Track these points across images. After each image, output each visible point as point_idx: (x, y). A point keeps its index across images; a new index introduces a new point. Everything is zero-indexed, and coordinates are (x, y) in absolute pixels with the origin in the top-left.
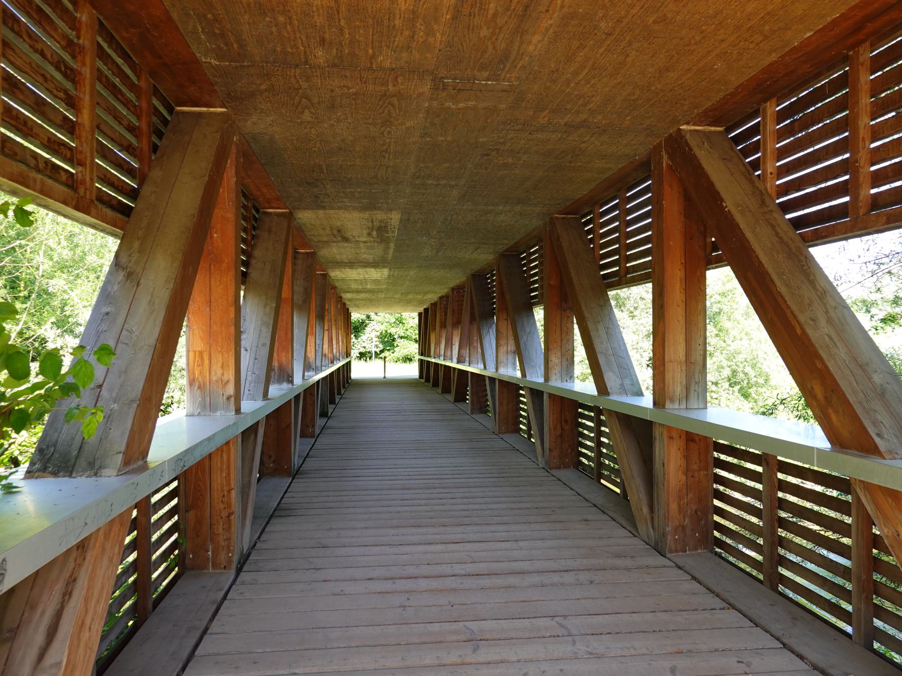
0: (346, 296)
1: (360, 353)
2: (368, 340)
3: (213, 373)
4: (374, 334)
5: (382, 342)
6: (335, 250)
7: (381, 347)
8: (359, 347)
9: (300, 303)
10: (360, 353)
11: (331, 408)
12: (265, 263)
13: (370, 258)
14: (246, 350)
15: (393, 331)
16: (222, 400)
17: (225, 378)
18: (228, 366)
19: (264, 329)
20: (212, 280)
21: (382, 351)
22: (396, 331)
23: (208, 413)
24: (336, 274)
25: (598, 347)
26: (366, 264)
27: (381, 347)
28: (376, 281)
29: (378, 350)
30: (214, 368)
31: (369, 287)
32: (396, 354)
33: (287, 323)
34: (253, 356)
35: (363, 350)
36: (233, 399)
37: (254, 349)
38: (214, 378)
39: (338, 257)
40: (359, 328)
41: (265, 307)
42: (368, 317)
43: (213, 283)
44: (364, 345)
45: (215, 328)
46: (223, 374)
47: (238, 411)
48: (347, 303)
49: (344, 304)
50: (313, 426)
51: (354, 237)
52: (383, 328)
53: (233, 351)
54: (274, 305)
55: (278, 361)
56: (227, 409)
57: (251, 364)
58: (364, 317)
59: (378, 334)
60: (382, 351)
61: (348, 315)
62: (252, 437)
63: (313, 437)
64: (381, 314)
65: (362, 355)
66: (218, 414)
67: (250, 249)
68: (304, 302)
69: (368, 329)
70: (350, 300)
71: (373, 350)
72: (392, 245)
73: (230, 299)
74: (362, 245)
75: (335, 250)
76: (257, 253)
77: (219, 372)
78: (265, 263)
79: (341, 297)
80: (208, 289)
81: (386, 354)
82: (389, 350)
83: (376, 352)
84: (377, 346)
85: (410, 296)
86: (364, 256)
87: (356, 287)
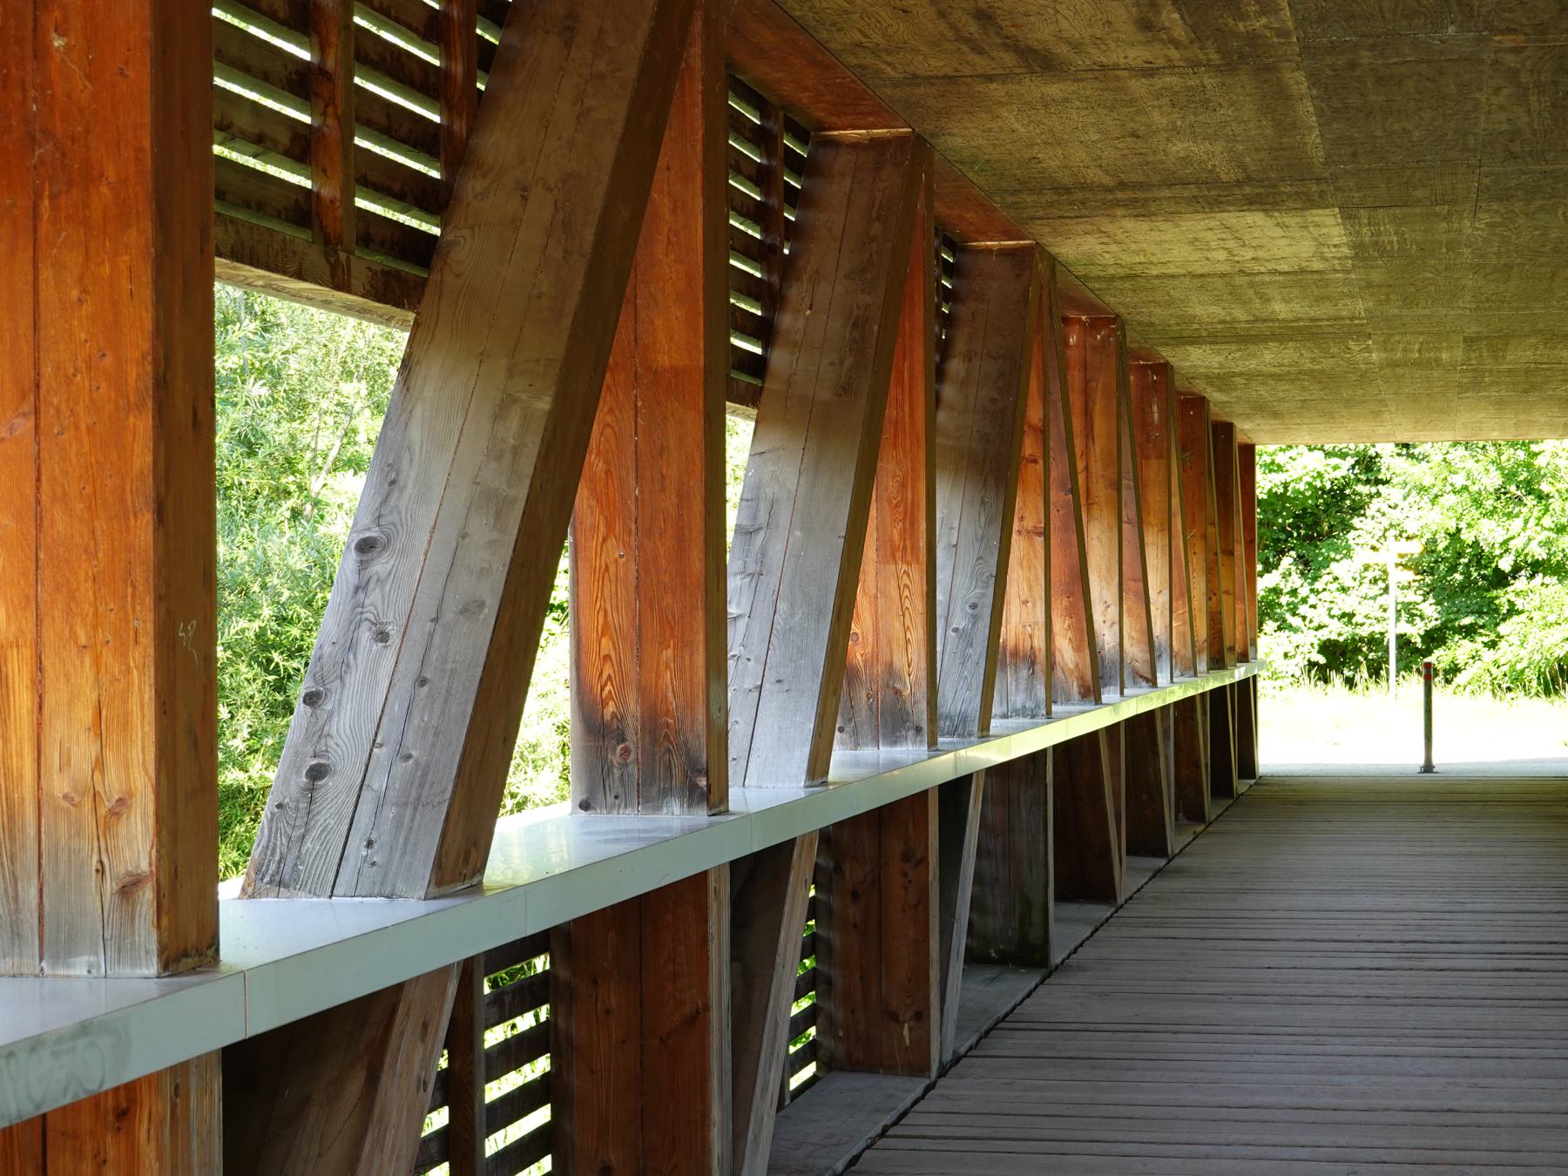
0: (1195, 362)
1: (1327, 648)
2: (1369, 580)
3: (53, 756)
4: (1391, 553)
5: (1440, 591)
6: (1011, 119)
7: (1431, 612)
8: (1319, 616)
9: (825, 395)
10: (1327, 648)
11: (1067, 927)
12: (524, 193)
13: (1212, 155)
14: (382, 637)
15: (1488, 532)
16: (95, 898)
17: (113, 785)
18: (126, 723)
19: (481, 529)
20: (46, 274)
21: (1435, 638)
22: (1506, 535)
23: (30, 963)
24: (1090, 248)
25: (1076, 561)
26: (1211, 193)
27: (1431, 612)
28: (1299, 279)
29: (1415, 632)
30: (57, 730)
31: (1280, 309)
32: (1505, 652)
33: (683, 496)
34: (410, 668)
35: (1337, 631)
36: (147, 895)
37: (420, 628)
38: (59, 785)
39: (1051, 160)
40: (1318, 523)
41: (498, 416)
42: (1367, 464)
43: (48, 293)
44: (1346, 603)
45: (60, 523)
46: (99, 765)
47: (190, 947)
48: (1214, 395)
49: (1200, 402)
50: (921, 1016)
51: (1077, 46)
52: (1434, 520)
53: (147, 640)
54: (544, 404)
55: (642, 691)
56: (121, 948)
57: (397, 708)
58: (1344, 468)
59: (1416, 548)
60: (1435, 638)
61: (1223, 461)
62: (355, 1086)
63: (916, 1066)
64: (1434, 448)
65: (1338, 658)
66: (79, 967)
67: (460, 127)
68: (845, 389)
69: (1364, 528)
70: (1223, 380)
71: (1392, 630)
72: (1297, 81)
73: (132, 372)
74: (1138, 86)
75: (1011, 119)
76: (497, 143)
77: (84, 750)
78: (524, 193)
79: (1165, 369)
80: (25, 323)
81: (1458, 650)
82: (1469, 632)
83: (1403, 642)
84: (1408, 611)
85: (1521, 354)
86: (1178, 148)
87: (1217, 311)
